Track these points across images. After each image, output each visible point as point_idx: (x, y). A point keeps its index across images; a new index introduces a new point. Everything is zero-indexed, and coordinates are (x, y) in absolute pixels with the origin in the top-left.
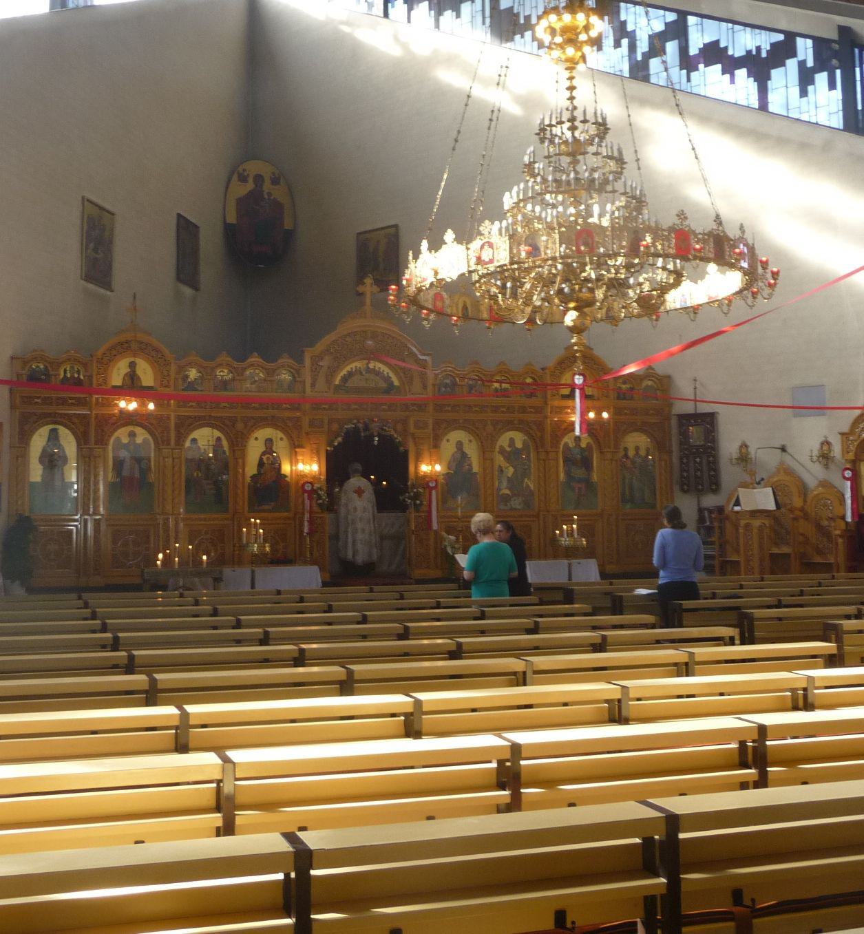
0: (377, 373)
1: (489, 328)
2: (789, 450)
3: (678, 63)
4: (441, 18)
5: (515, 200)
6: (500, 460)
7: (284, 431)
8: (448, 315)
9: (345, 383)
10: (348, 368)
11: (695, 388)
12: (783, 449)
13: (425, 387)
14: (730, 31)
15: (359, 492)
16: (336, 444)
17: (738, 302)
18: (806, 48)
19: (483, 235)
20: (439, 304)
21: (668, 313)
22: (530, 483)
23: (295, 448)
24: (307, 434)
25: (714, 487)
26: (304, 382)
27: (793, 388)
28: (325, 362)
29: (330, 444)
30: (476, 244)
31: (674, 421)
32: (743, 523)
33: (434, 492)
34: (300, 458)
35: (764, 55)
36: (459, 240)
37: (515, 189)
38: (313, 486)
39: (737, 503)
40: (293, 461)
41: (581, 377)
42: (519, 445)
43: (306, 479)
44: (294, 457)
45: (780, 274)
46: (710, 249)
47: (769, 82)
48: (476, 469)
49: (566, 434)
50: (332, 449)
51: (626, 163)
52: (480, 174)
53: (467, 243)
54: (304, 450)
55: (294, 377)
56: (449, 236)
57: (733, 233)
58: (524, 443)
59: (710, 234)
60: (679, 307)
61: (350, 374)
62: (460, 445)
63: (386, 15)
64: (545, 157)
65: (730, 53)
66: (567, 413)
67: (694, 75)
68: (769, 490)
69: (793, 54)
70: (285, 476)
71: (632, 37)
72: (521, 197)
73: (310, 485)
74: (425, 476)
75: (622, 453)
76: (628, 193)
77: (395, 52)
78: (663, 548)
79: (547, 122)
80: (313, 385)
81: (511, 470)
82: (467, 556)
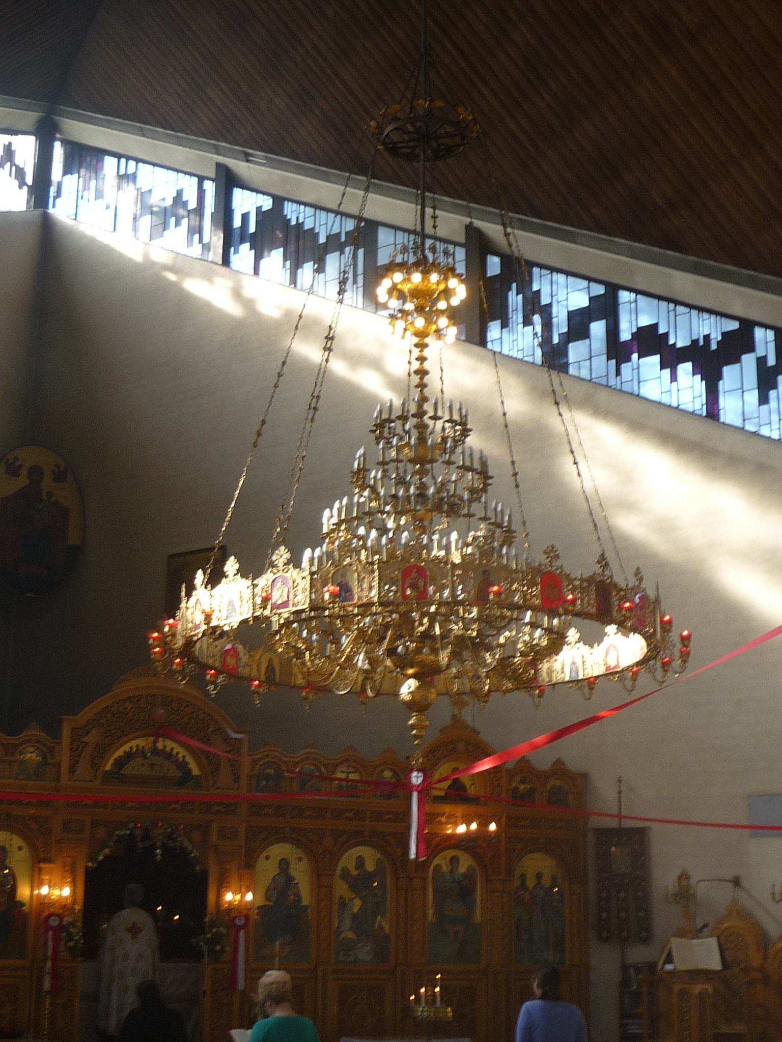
0: (169, 756)
1: (306, 698)
2: (744, 882)
3: (604, 349)
4: (300, 271)
5: (335, 520)
6: (341, 889)
7: (25, 838)
8: (246, 679)
9: (120, 769)
10: (126, 748)
11: (620, 793)
12: (736, 882)
13: (237, 779)
14: (672, 314)
15: (134, 930)
16: (101, 858)
17: (644, 678)
18: (767, 343)
19: (276, 566)
20: (231, 661)
21: (554, 688)
22: (385, 924)
23: (39, 862)
24: (59, 842)
25: (644, 934)
26: (59, 766)
27: (749, 796)
28: (92, 738)
29: (92, 858)
30: (264, 580)
31: (591, 838)
32: (677, 988)
33: (242, 934)
34: (46, 877)
35: (714, 346)
36: (243, 572)
37: (337, 505)
38: (61, 919)
39: (669, 960)
40: (36, 883)
41: (421, 774)
42: (370, 867)
43: (52, 910)
44: (36, 876)
45: (692, 639)
46: (590, 603)
47: (721, 383)
48: (306, 901)
49: (439, 853)
50: (95, 865)
51: (491, 477)
52: (298, 480)
53: (253, 580)
54: (52, 865)
55: (44, 757)
56: (231, 565)
57: (622, 578)
58: (379, 864)
59: (590, 580)
60: (567, 679)
61: (129, 756)
62: (284, 865)
63: (226, 261)
64: (379, 463)
65: (671, 342)
66: (440, 823)
67: (625, 368)
68: (713, 942)
69: (751, 348)
70: (22, 904)
71: (546, 312)
72: (343, 517)
73: (57, 918)
74: (231, 908)
75: (517, 882)
76: (490, 519)
77: (234, 309)
78: (529, 1029)
79: (385, 416)
80: (72, 770)
81: (358, 903)
82: (250, 1032)
